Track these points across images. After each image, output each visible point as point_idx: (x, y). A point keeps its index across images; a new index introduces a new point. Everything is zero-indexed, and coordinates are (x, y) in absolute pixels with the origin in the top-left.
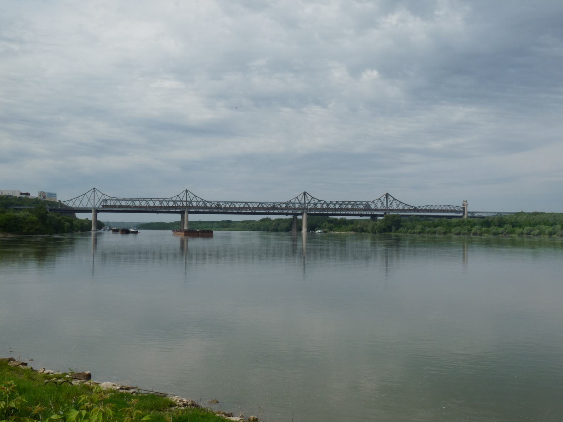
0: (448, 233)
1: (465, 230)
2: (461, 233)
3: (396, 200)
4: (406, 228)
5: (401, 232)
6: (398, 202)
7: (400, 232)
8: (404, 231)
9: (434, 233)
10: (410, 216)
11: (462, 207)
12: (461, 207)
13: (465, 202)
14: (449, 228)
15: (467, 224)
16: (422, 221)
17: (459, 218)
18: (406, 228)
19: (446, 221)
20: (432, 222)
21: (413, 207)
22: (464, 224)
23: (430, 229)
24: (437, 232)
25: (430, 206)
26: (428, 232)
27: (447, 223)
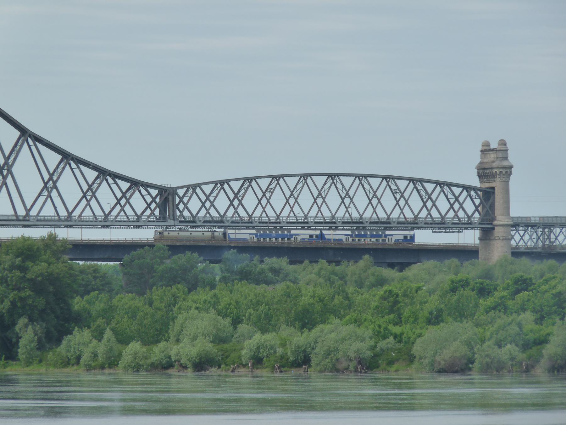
0: (391, 363)
1: (499, 345)
2: (477, 365)
3: (37, 139)
4: (108, 333)
5: (78, 358)
6: (53, 159)
7: (67, 363)
8: (95, 355)
9: (297, 364)
10: (140, 251)
11: (475, 189)
12: (466, 188)
13: (493, 156)
14: (397, 330)
15: (509, 303)
16: (213, 286)
17: (454, 261)
18: (108, 333)
19: (373, 285)
20: (280, 287)
21: (154, 192)
22: (490, 301)
23: (268, 336)
24: (314, 360)
25: (264, 183)
26: (258, 361)
27: (383, 298)
